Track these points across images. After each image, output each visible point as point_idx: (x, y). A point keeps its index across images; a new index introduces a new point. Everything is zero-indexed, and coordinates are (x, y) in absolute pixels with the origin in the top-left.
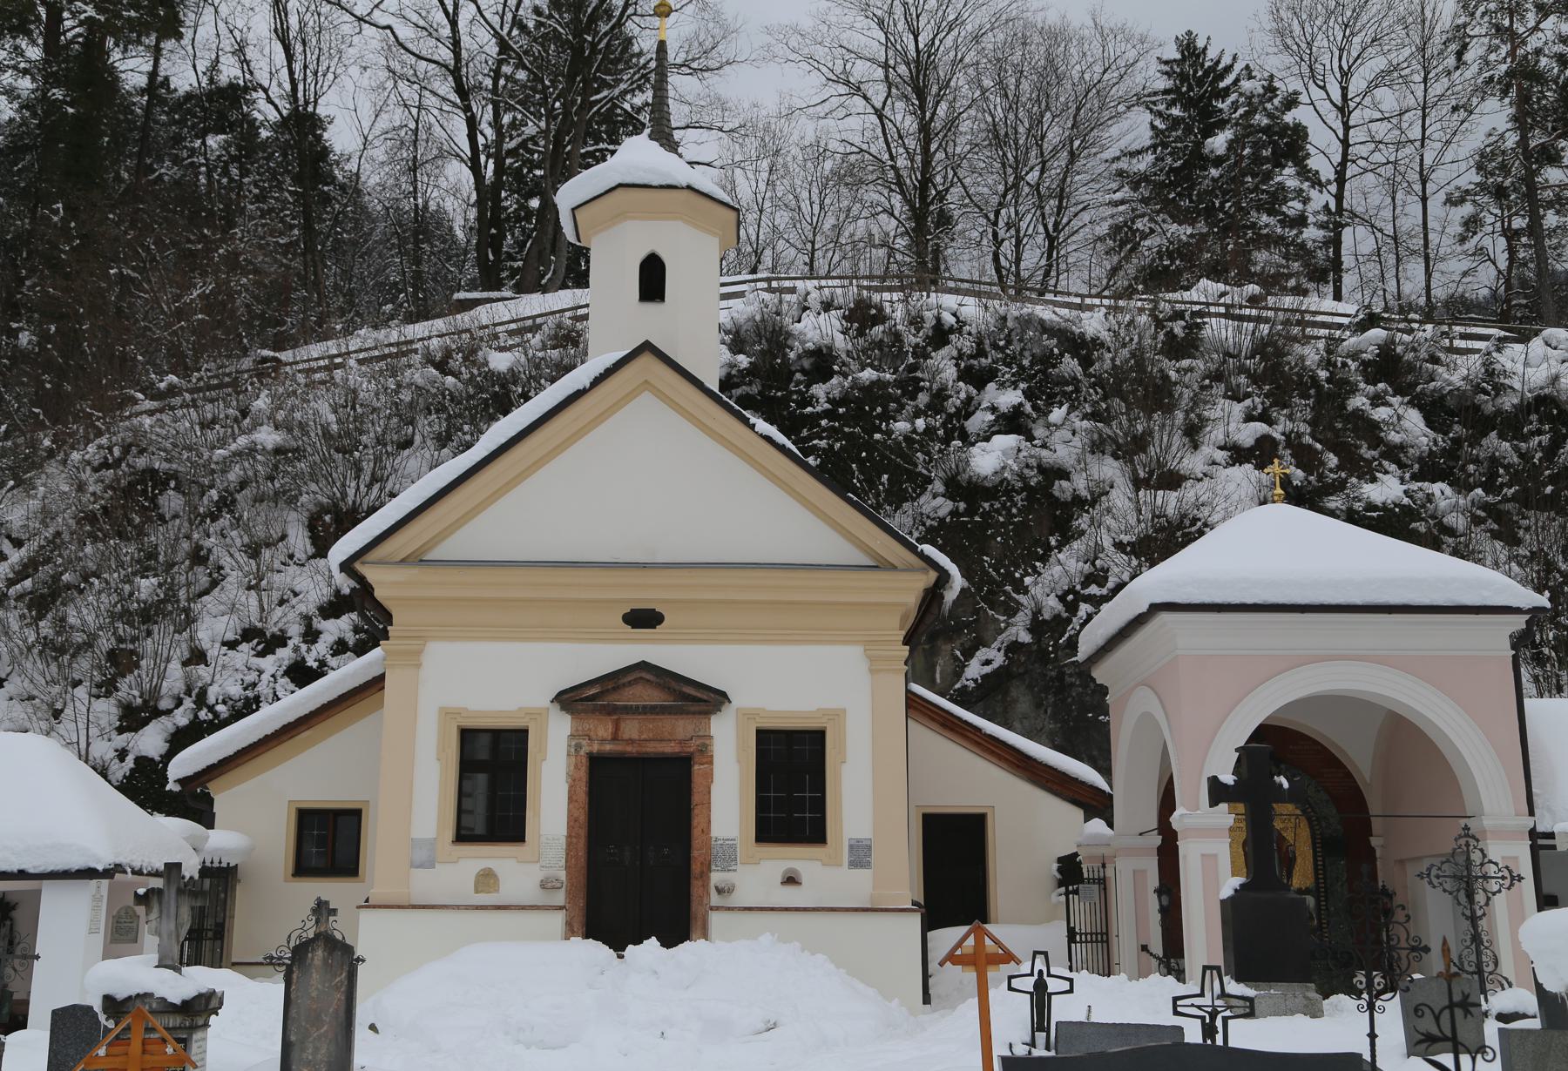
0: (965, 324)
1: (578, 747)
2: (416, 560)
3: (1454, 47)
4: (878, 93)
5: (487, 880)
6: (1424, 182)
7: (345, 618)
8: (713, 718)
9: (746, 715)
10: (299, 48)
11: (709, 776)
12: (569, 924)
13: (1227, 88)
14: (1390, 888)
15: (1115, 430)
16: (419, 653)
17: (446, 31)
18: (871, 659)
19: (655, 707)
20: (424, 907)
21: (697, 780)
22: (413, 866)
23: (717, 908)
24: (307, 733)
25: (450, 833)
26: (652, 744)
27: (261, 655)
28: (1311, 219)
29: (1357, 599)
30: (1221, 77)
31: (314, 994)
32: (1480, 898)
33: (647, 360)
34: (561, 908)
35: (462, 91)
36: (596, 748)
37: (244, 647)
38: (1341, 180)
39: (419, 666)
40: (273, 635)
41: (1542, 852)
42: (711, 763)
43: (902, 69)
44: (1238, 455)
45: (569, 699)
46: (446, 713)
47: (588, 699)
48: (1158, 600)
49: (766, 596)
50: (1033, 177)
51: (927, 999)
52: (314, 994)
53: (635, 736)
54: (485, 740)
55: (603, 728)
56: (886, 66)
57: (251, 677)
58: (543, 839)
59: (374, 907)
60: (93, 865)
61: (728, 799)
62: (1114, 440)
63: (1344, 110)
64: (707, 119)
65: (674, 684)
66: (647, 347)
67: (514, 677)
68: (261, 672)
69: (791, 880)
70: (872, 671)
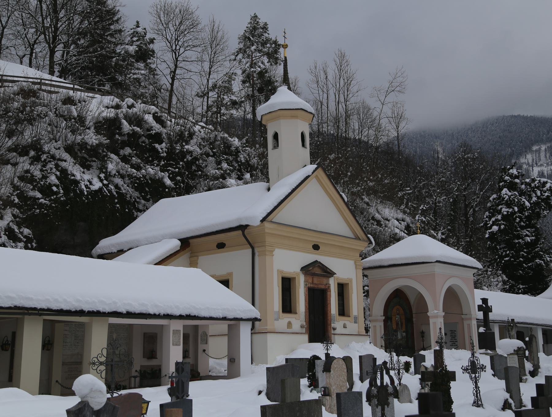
1: (306, 285)
5: (289, 324)
9: (338, 278)
16: (272, 251)
36: (309, 285)
41: (250, 323)
51: (252, 363)
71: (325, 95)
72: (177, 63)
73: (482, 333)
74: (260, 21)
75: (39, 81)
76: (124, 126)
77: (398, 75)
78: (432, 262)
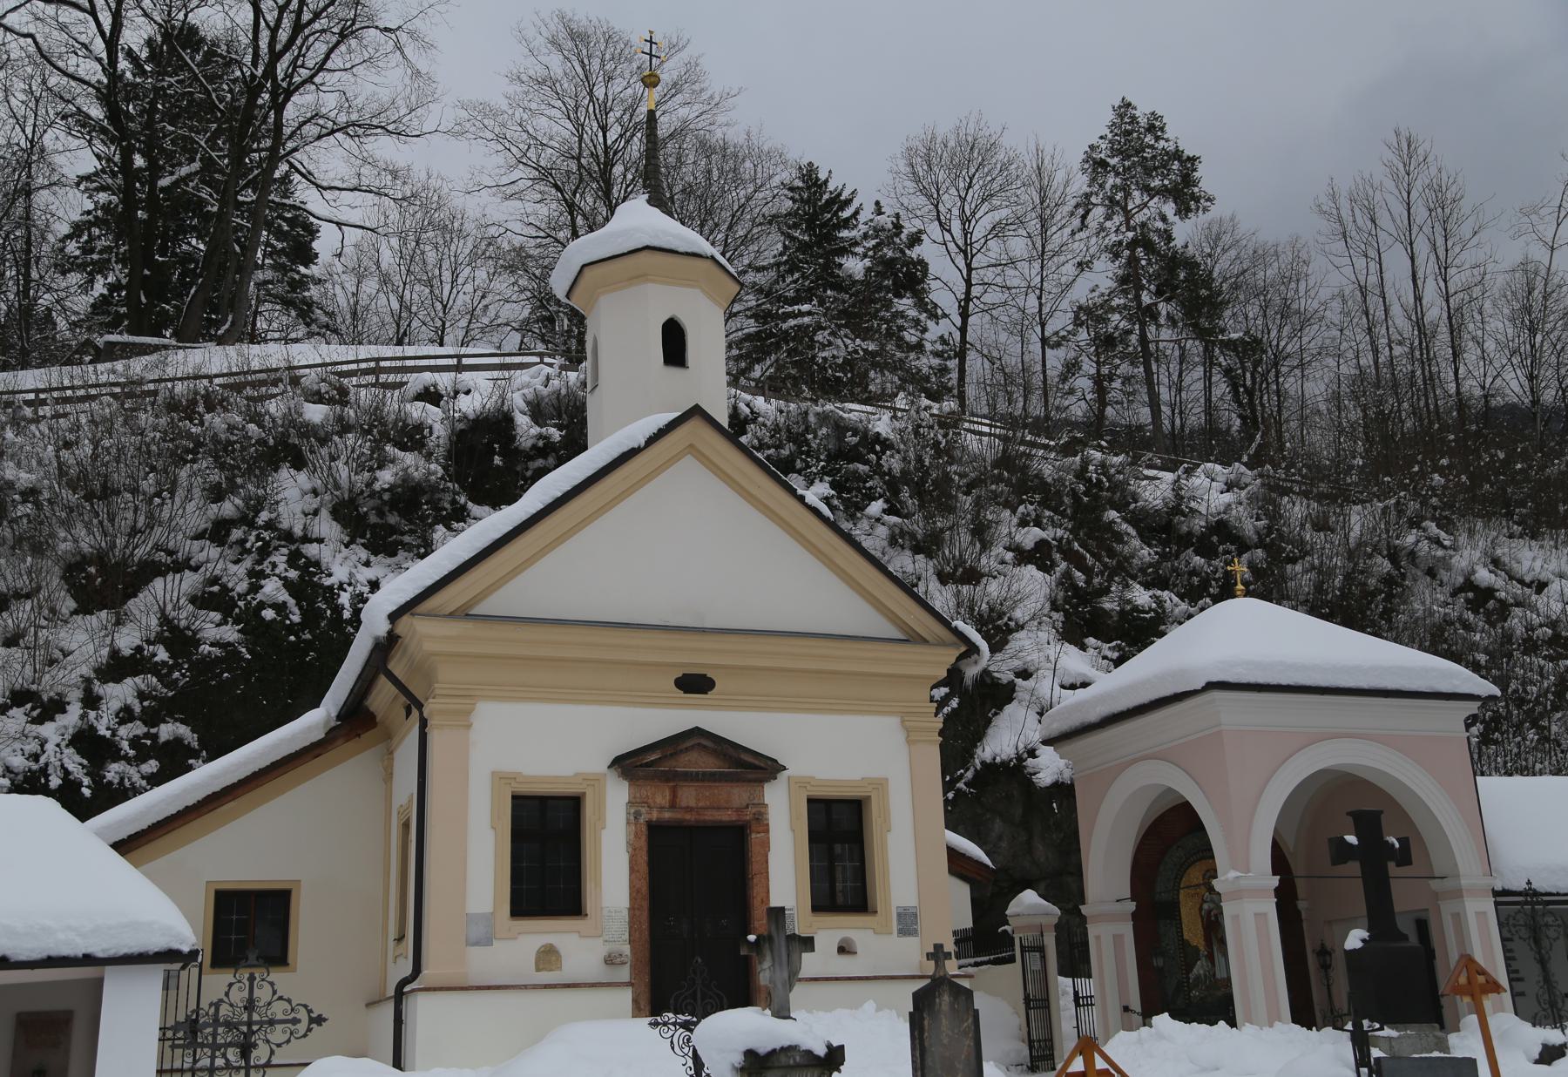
0: (759, 414)
1: (637, 815)
2: (463, 614)
3: (1081, 211)
5: (548, 957)
7: (129, 681)
8: (766, 786)
9: (802, 783)
11: (766, 845)
12: (635, 1001)
13: (847, 220)
15: (917, 526)
16: (468, 713)
18: (908, 731)
19: (713, 774)
21: (755, 849)
24: (232, 804)
26: (709, 812)
27: (39, 721)
28: (928, 347)
29: (1364, 683)
30: (842, 209)
33: (695, 425)
36: (655, 816)
37: (15, 712)
38: (965, 315)
39: (469, 726)
40: (51, 699)
42: (767, 831)
44: (1024, 557)
45: (629, 764)
46: (499, 778)
48: (1215, 679)
49: (807, 665)
53: (692, 803)
55: (661, 797)
57: (33, 747)
58: (605, 912)
60: (175, 946)
61: (785, 875)
62: (912, 535)
63: (966, 251)
64: (909, 184)
67: (569, 740)
68: (43, 743)
70: (909, 742)
71: (1373, 266)
72: (969, 275)
74: (1137, 113)
75: (372, 364)
76: (519, 431)
78: (1194, 693)
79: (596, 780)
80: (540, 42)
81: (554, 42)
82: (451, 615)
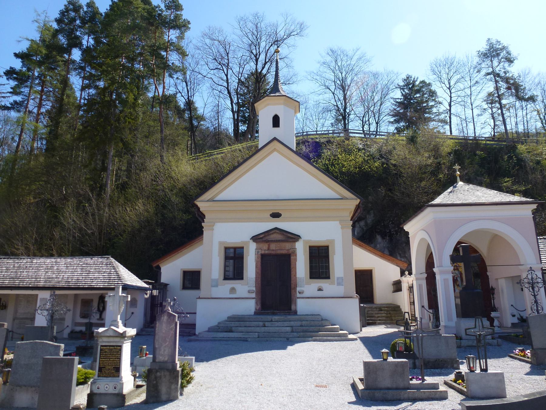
1: (258, 252)
2: (212, 200)
4: (332, 88)
5: (233, 290)
6: (472, 105)
9: (305, 242)
10: (189, 83)
11: (296, 260)
14: (494, 287)
17: (225, 78)
20: (215, 298)
21: (292, 261)
22: (212, 286)
23: (299, 298)
25: (222, 277)
31: (164, 331)
32: (536, 289)
33: (275, 142)
34: (254, 298)
35: (229, 93)
36: (263, 252)
39: (213, 229)
41: (544, 275)
43: (338, 82)
45: (255, 239)
46: (221, 243)
47: (260, 238)
49: (309, 207)
50: (372, 109)
52: (164, 331)
54: (232, 250)
55: (265, 246)
56: (335, 82)
59: (201, 298)
65: (285, 233)
66: (275, 139)
69: (320, 290)
73: (42, 328)
77: (293, 34)
79: (247, 243)
80: (324, 54)
81: (328, 54)
82: (208, 201)
